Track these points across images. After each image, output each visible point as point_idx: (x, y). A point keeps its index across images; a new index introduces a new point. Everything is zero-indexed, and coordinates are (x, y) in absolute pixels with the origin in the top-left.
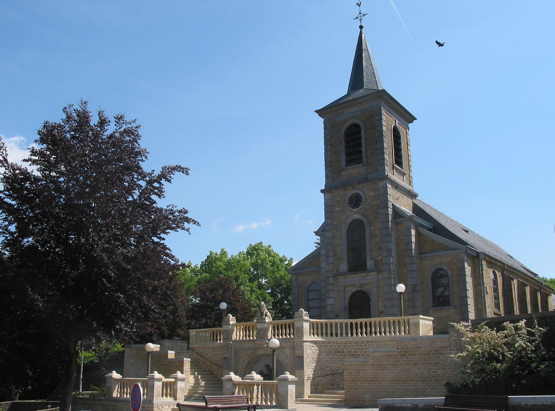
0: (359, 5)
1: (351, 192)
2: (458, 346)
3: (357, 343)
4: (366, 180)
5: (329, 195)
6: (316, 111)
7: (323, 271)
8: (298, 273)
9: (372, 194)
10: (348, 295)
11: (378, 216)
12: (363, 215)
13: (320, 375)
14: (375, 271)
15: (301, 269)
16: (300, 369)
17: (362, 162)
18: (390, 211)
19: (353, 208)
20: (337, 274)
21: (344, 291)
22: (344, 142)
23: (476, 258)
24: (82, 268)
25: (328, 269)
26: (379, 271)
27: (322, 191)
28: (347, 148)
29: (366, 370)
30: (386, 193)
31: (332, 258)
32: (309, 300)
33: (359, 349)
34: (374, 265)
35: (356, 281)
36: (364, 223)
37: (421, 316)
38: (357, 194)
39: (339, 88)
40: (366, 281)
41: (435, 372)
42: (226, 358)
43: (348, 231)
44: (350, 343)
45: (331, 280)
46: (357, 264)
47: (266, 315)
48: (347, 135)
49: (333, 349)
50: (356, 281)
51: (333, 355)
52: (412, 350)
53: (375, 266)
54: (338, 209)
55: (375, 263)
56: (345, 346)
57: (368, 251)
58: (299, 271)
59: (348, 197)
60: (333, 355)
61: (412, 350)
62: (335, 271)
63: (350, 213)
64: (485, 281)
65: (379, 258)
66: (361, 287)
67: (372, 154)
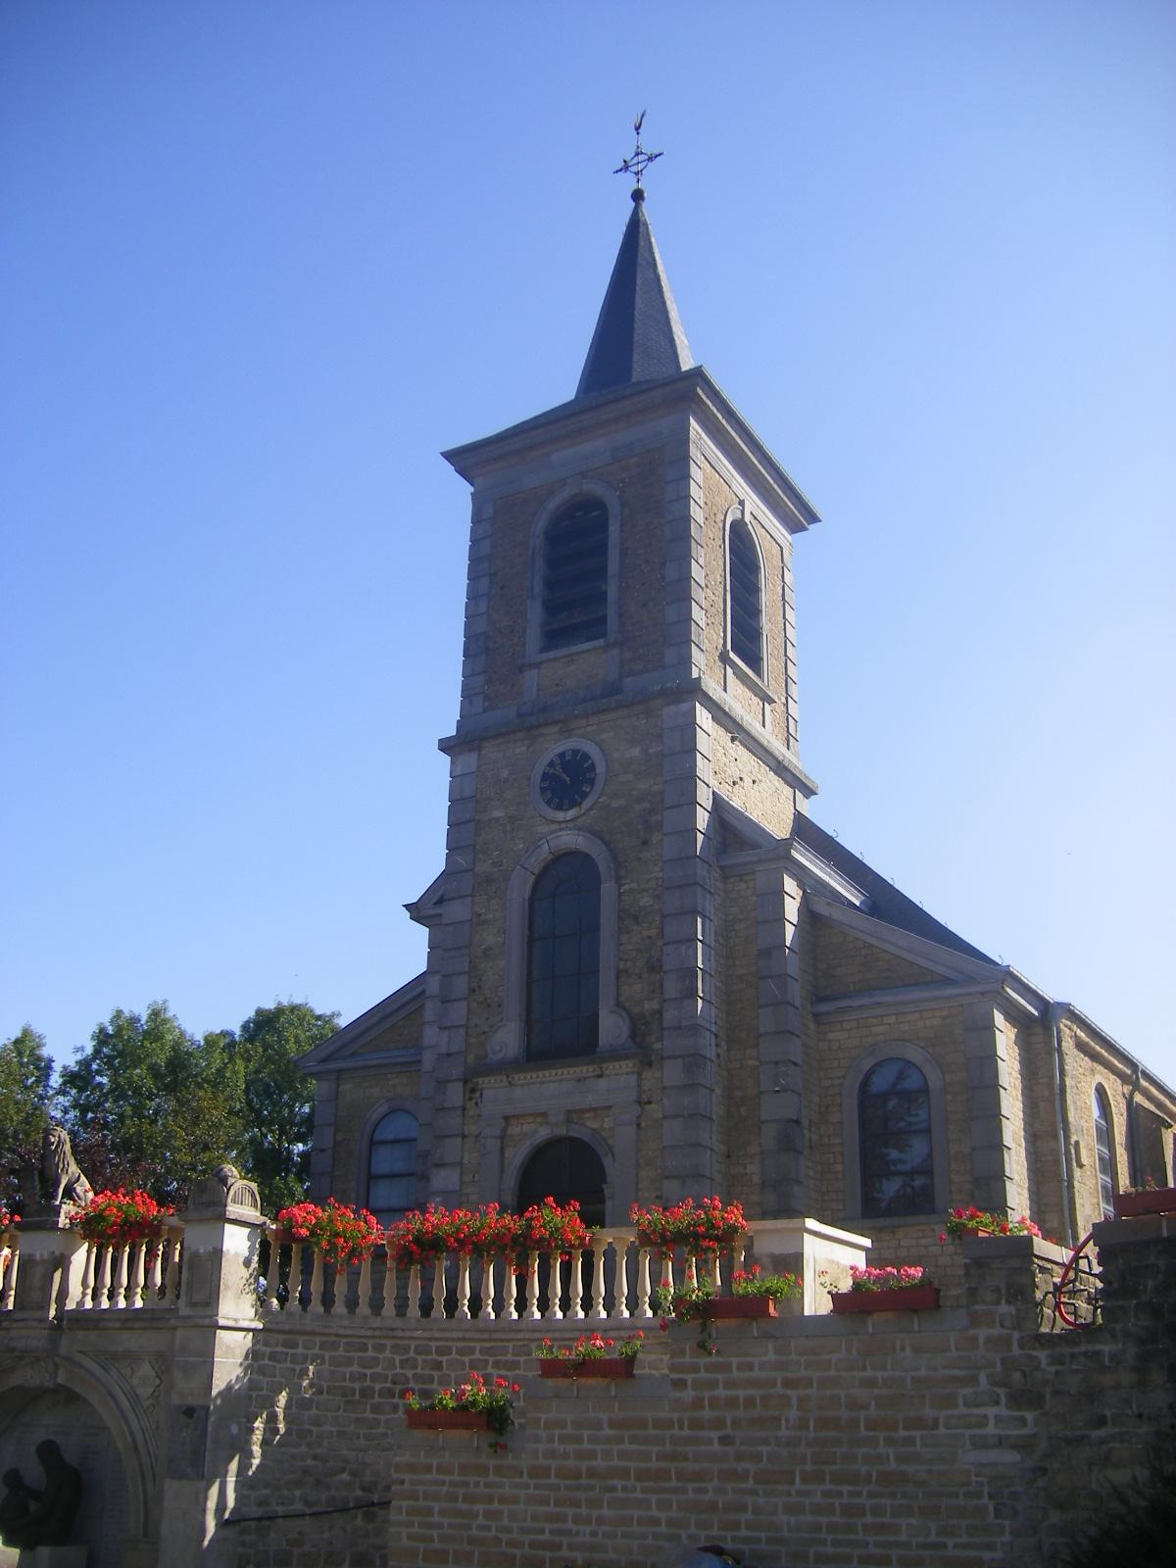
1: (554, 746)
2: (1017, 1376)
4: (607, 697)
5: (470, 760)
6: (449, 456)
7: (428, 1060)
8: (339, 1071)
10: (517, 1155)
11: (655, 838)
13: (298, 1507)
14: (627, 1057)
15: (354, 1054)
17: (604, 635)
18: (702, 819)
19: (560, 808)
20: (477, 1071)
22: (540, 563)
23: (1041, 1023)
25: (443, 1050)
26: (647, 1060)
27: (445, 746)
28: (550, 585)
29: (503, 1500)
32: (372, 1177)
35: (548, 1100)
36: (587, 856)
37: (811, 1223)
39: (553, 376)
41: (882, 1528)
43: (532, 899)
46: (561, 1035)
48: (553, 537)
49: (375, 1377)
50: (548, 1100)
51: (376, 1408)
53: (633, 1036)
54: (497, 814)
57: (606, 977)
58: (342, 1065)
60: (376, 1408)
62: (471, 1058)
63: (543, 829)
64: (1071, 1119)
65: (650, 1006)
66: (569, 1121)
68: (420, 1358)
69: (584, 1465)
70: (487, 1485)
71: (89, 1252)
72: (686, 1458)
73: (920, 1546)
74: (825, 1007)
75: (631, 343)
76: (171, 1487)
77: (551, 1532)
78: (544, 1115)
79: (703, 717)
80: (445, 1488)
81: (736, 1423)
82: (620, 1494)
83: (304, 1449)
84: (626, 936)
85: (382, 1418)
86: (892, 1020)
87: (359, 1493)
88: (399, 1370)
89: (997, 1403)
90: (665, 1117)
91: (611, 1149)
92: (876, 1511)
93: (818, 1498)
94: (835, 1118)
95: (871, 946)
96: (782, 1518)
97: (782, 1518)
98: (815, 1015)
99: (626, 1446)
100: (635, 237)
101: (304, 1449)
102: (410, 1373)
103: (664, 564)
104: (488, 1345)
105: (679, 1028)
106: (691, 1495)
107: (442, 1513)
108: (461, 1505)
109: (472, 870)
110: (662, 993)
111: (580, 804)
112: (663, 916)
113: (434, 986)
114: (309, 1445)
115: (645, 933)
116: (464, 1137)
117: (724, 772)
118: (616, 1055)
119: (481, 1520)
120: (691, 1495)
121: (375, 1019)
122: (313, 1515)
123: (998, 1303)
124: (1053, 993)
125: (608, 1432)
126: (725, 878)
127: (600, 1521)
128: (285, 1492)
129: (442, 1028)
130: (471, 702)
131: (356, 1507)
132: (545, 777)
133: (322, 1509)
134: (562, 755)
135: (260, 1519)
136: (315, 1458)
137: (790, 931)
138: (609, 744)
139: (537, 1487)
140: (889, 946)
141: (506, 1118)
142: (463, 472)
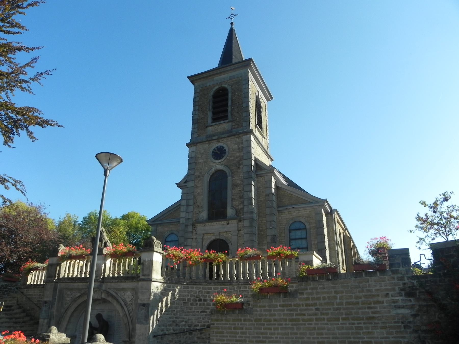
1: (215, 145)
4: (230, 134)
5: (194, 148)
7: (182, 221)
8: (157, 224)
11: (241, 166)
12: (226, 166)
13: (172, 331)
14: (235, 219)
15: (161, 220)
16: (142, 323)
17: (228, 119)
19: (217, 159)
21: (203, 239)
22: (211, 102)
24: (163, 327)
27: (188, 145)
28: (214, 108)
30: (250, 146)
31: (192, 207)
34: (234, 213)
36: (225, 172)
39: (212, 61)
43: (210, 182)
45: (190, 229)
46: (217, 212)
48: (215, 96)
49: (192, 296)
50: (216, 229)
52: (326, 295)
53: (236, 214)
54: (201, 161)
55: (236, 211)
56: (208, 293)
61: (326, 295)
62: (194, 220)
63: (213, 164)
67: (238, 112)
68: (203, 290)
69: (272, 318)
70: (241, 324)
71: (111, 261)
72: (304, 315)
73: (381, 338)
74: (280, 209)
75: (232, 54)
76: (138, 326)
77: (263, 337)
78: (213, 233)
79: (252, 138)
80: (228, 326)
81: (321, 304)
82: (284, 326)
83: (173, 315)
85: (194, 307)
86: (297, 212)
87: (187, 327)
88: (198, 294)
89: (402, 296)
91: (231, 242)
92: (367, 328)
93: (348, 325)
94: (283, 235)
96: (336, 331)
97: (336, 331)
98: (278, 211)
99: (286, 312)
100: (231, 33)
101: (173, 315)
102: (201, 295)
106: (307, 325)
107: (227, 333)
108: (233, 330)
113: (184, 203)
114: (174, 314)
116: (192, 239)
117: (257, 153)
119: (240, 335)
120: (307, 325)
122: (176, 333)
123: (399, 267)
124: (333, 207)
125: (279, 308)
126: (257, 177)
127: (278, 334)
128: (168, 327)
129: (187, 212)
131: (187, 331)
132: (213, 152)
133: (178, 332)
134: (217, 147)
135: (162, 335)
136: (176, 318)
137: (273, 190)
138: (229, 144)
139: (257, 324)
140: (292, 195)
141: (203, 234)
142: (192, 82)
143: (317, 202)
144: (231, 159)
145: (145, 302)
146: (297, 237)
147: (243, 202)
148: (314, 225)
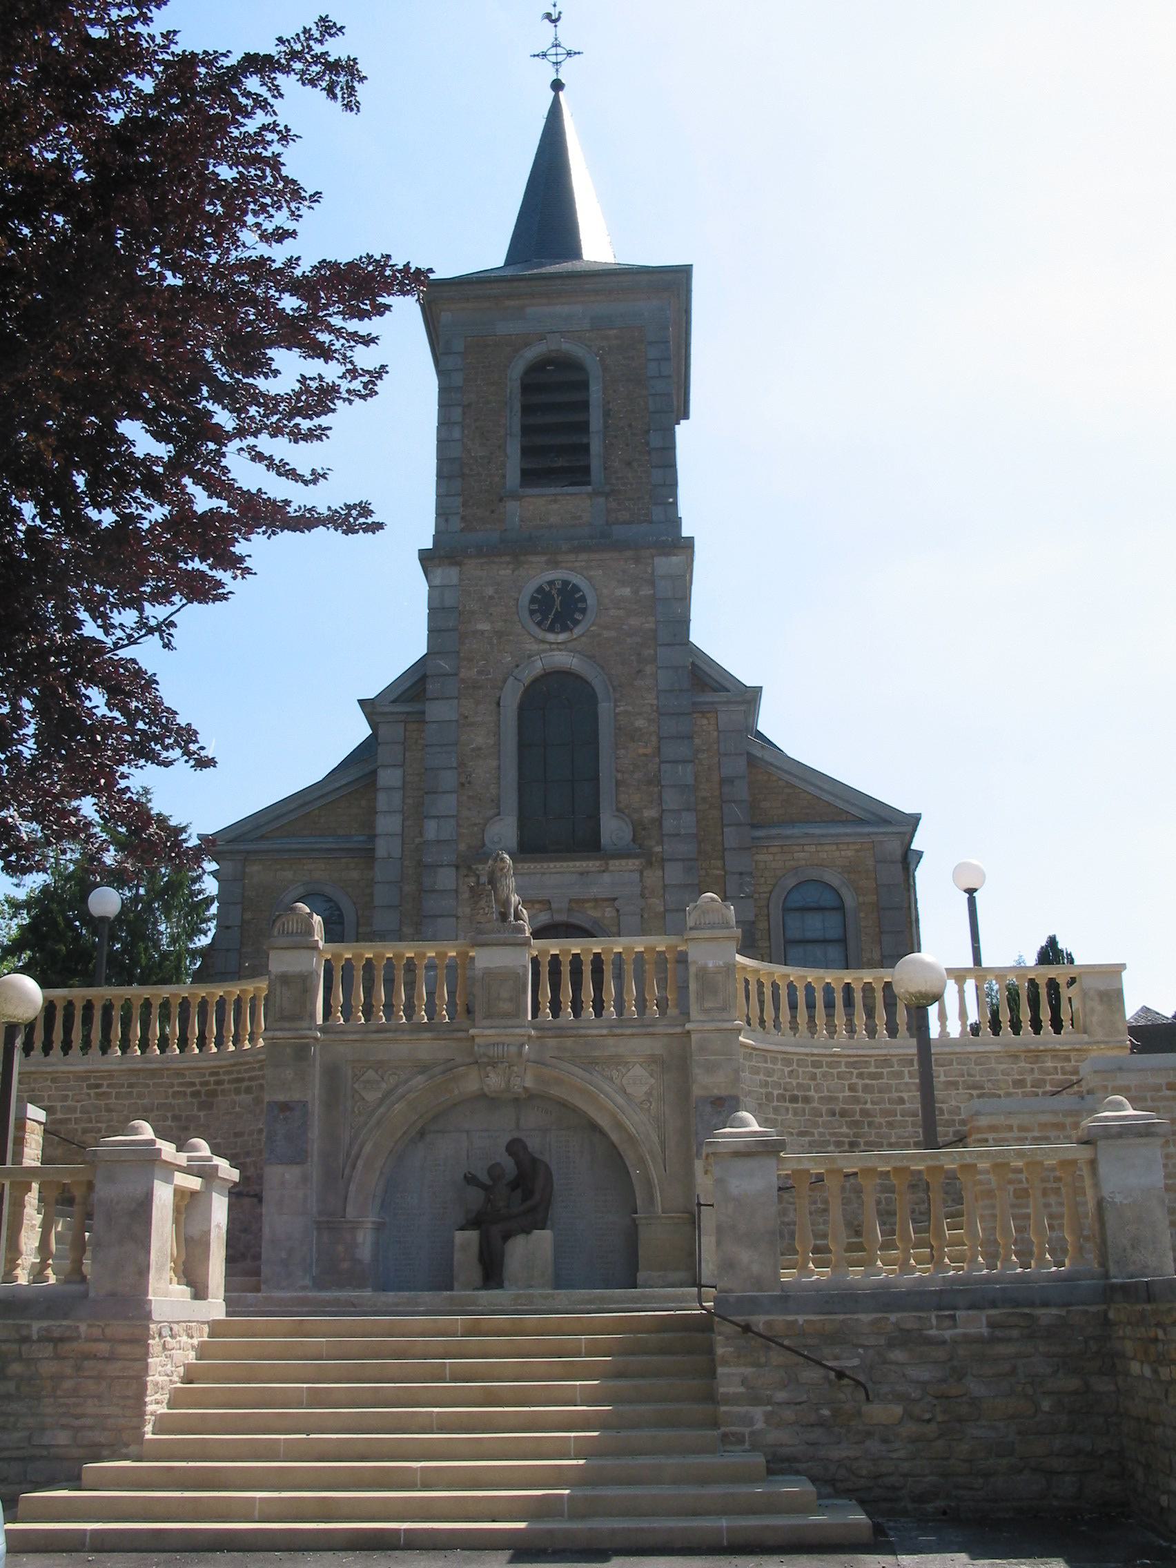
0: (553, 19)
3: (856, 1063)
4: (601, 541)
5: (451, 575)
8: (248, 852)
9: (627, 591)
11: (649, 669)
14: (628, 856)
15: (262, 837)
19: (551, 629)
26: (650, 861)
33: (866, 1088)
34: (628, 835)
38: (566, 583)
40: (595, 891)
42: (285, 1107)
44: (829, 1065)
47: (518, 917)
53: (634, 840)
54: (484, 626)
59: (530, 588)
60: (776, 1110)
62: (462, 847)
63: (535, 647)
65: (650, 813)
67: (629, 464)
84: (623, 751)
85: (779, 1118)
86: (813, 848)
90: (666, 911)
95: (794, 786)
103: (648, 432)
104: (852, 1060)
105: (678, 835)
109: (456, 675)
110: (660, 804)
111: (571, 630)
112: (660, 739)
115: (641, 751)
118: (621, 854)
121: (293, 806)
130: (447, 520)
138: (601, 582)
143: (886, 822)
144: (606, 634)
145: (724, 1093)
146: (809, 935)
147: (660, 797)
148: (872, 898)
